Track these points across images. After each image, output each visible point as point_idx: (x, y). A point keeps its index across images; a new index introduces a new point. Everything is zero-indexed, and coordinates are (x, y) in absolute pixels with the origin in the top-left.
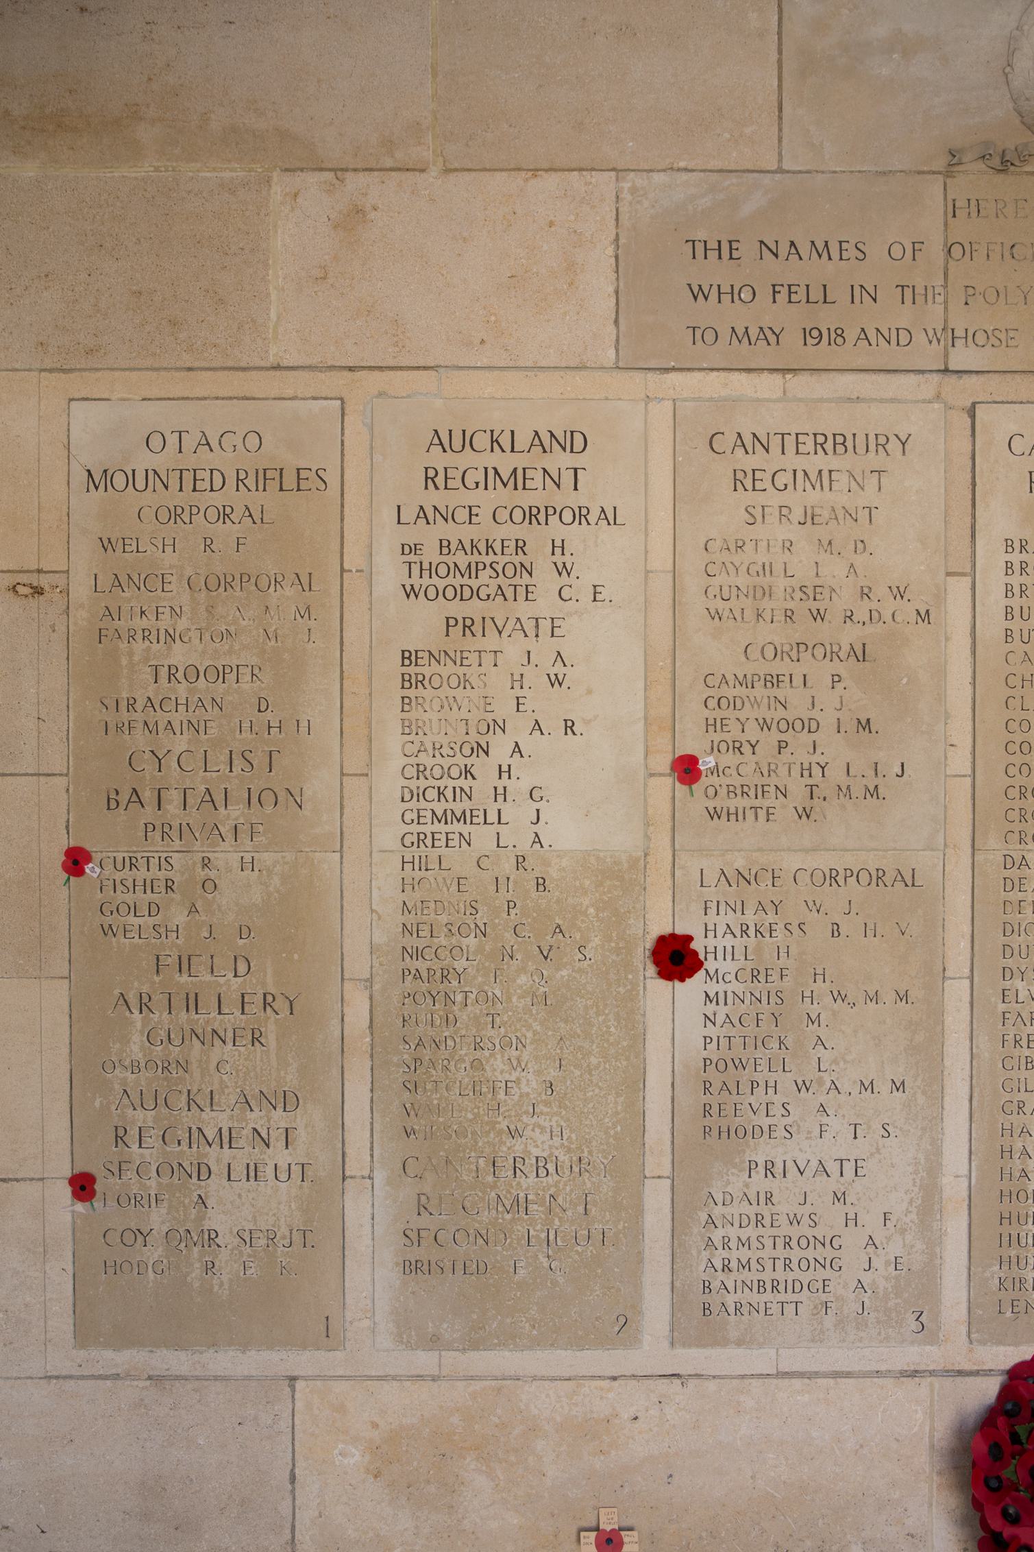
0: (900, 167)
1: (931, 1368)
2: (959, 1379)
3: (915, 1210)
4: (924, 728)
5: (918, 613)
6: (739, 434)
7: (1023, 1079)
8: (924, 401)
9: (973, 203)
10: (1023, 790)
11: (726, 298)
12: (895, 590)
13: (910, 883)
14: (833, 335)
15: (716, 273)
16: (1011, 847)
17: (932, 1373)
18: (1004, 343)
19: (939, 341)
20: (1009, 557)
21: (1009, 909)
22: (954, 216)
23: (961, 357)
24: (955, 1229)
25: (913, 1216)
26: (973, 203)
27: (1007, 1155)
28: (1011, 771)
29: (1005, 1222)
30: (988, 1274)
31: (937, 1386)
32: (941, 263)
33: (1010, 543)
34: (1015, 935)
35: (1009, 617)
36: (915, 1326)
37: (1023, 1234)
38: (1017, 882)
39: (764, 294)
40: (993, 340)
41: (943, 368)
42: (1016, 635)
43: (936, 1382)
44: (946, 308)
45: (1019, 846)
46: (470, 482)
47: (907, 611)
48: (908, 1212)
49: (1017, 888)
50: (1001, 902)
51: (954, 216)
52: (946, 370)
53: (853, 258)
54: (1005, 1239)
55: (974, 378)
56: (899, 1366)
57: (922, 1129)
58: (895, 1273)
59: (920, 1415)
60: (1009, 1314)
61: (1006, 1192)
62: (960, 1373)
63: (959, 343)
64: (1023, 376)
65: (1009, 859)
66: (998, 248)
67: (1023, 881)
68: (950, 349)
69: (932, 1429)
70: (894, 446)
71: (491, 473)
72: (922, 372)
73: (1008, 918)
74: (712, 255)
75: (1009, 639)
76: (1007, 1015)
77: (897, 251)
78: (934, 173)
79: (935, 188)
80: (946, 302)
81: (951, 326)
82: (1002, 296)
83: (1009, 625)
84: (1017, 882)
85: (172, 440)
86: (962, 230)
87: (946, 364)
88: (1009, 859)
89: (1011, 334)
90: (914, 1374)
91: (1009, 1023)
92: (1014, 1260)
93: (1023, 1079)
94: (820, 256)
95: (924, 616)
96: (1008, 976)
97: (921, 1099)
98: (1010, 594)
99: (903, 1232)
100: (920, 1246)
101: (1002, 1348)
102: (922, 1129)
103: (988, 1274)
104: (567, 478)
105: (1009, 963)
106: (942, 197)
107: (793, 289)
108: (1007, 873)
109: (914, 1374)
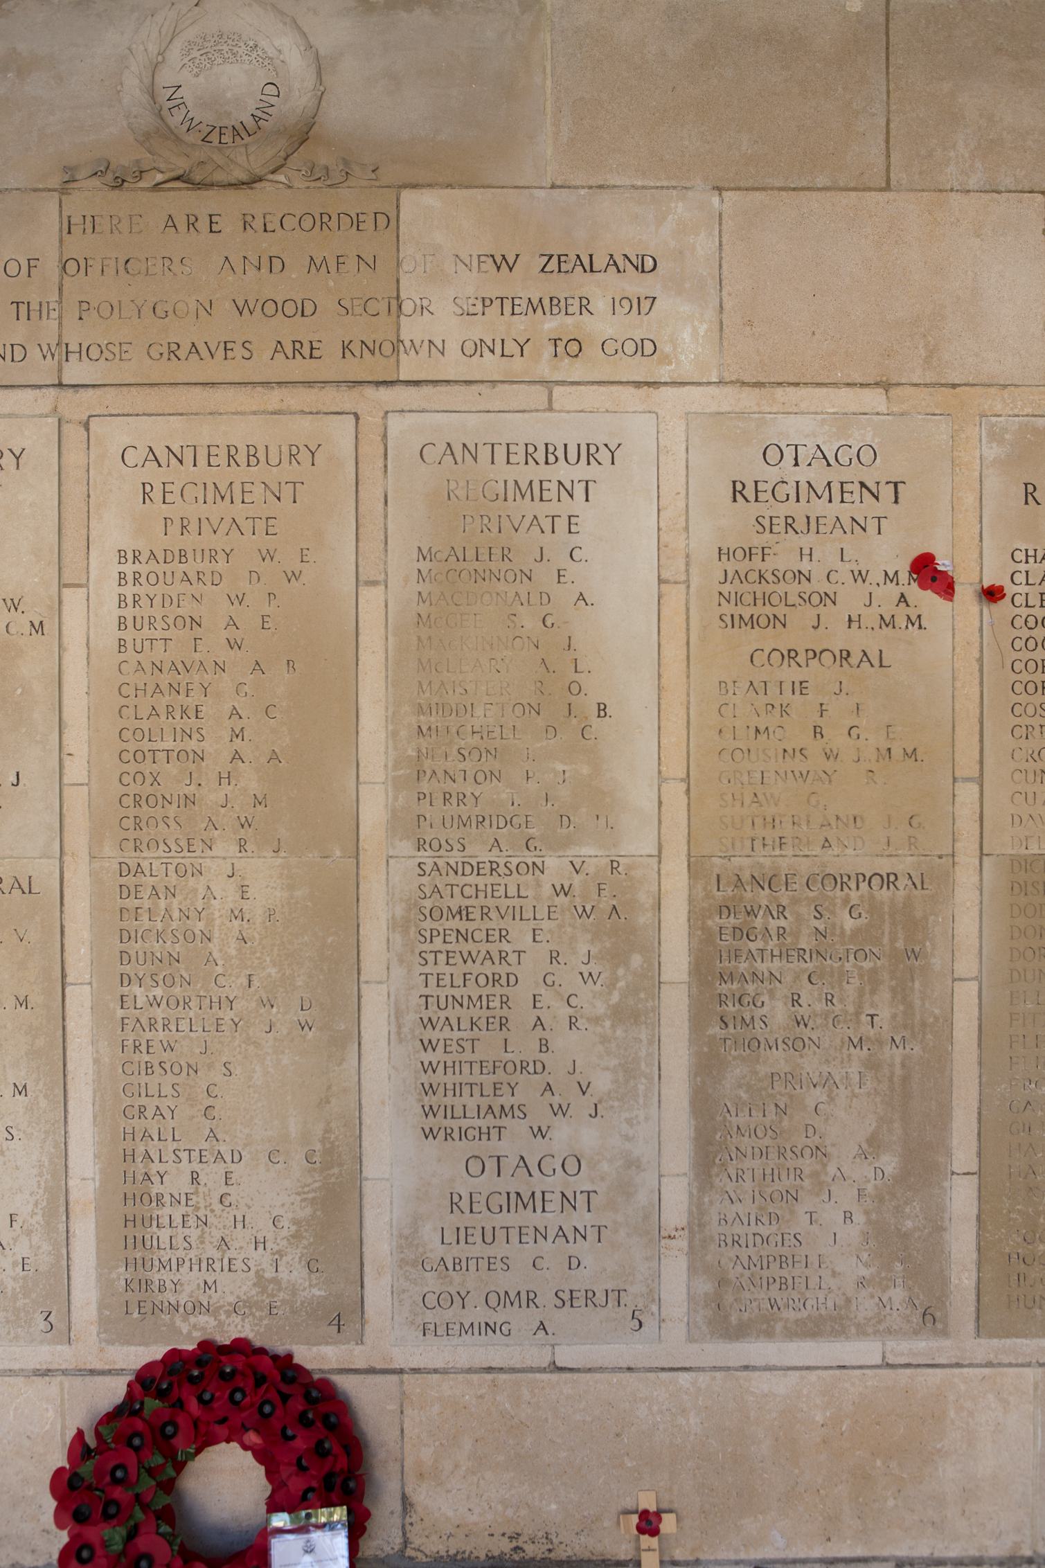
0: (16, 186)
1: (63, 1367)
2: (88, 1379)
3: (40, 1212)
4: (38, 738)
5: (33, 625)
6: (449, 444)
7: (143, 1084)
8: (41, 416)
9: (89, 219)
10: (138, 798)
12: (9, 603)
13: (27, 890)
16: (126, 854)
17: (64, 1372)
18: (118, 356)
19: (53, 355)
20: (122, 568)
21: (125, 916)
22: (69, 232)
23: (76, 371)
24: (85, 1232)
25: (39, 1218)
26: (89, 219)
27: (129, 1158)
28: (126, 779)
29: (130, 1224)
30: (114, 1275)
31: (66, 1385)
32: (56, 279)
33: (123, 554)
34: (132, 942)
35: (123, 627)
36: (43, 1325)
37: (147, 1237)
38: (133, 890)
40: (106, 354)
41: (57, 382)
42: (130, 645)
43: (67, 1381)
44: (60, 324)
45: (134, 854)
46: (781, 495)
47: (21, 623)
48: (33, 1214)
49: (133, 895)
50: (118, 909)
51: (69, 232)
52: (60, 385)
54: (130, 1241)
55: (91, 391)
56: (32, 1365)
57: (45, 1132)
58: (22, 1273)
59: (51, 1414)
60: (136, 1315)
61: (130, 1196)
62: (92, 1372)
63: (73, 358)
64: (139, 388)
65: (124, 867)
66: (113, 263)
67: (139, 889)
68: (64, 363)
69: (64, 1427)
70: (604, 455)
72: (40, 387)
73: (124, 924)
75: (123, 649)
76: (126, 1021)
77: (13, 268)
78: (49, 190)
79: (50, 205)
80: (60, 317)
81: (65, 341)
82: (116, 310)
83: (122, 634)
84: (133, 890)
85: (789, 454)
86: (78, 246)
87: (60, 378)
88: (124, 867)
89: (125, 348)
90: (47, 1373)
91: (128, 1028)
92: (140, 1262)
93: (143, 1084)
95: (38, 628)
96: (126, 982)
97: (43, 1103)
98: (123, 604)
99: (29, 1233)
100: (46, 1247)
101: (133, 1348)
102: (45, 1132)
103: (114, 1275)
104: (579, 491)
105: (127, 969)
106: (57, 214)
108: (123, 881)
109: (47, 1373)
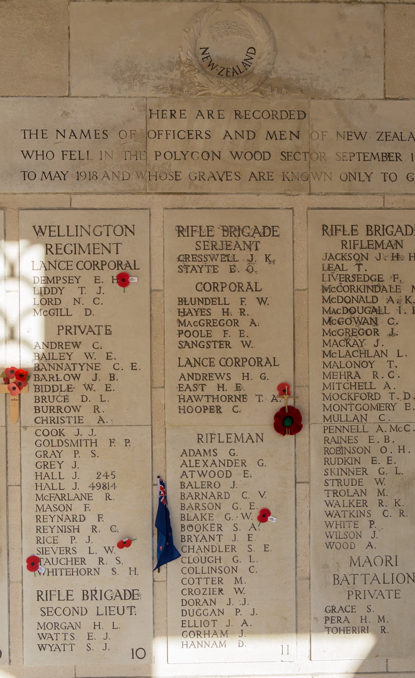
11: (40, 158)
14: (92, 175)
15: (34, 144)
39: (58, 155)
46: (68, 251)
53: (234, 179)
71: (77, 246)
74: (34, 136)
94: (86, 137)
107: (72, 153)
